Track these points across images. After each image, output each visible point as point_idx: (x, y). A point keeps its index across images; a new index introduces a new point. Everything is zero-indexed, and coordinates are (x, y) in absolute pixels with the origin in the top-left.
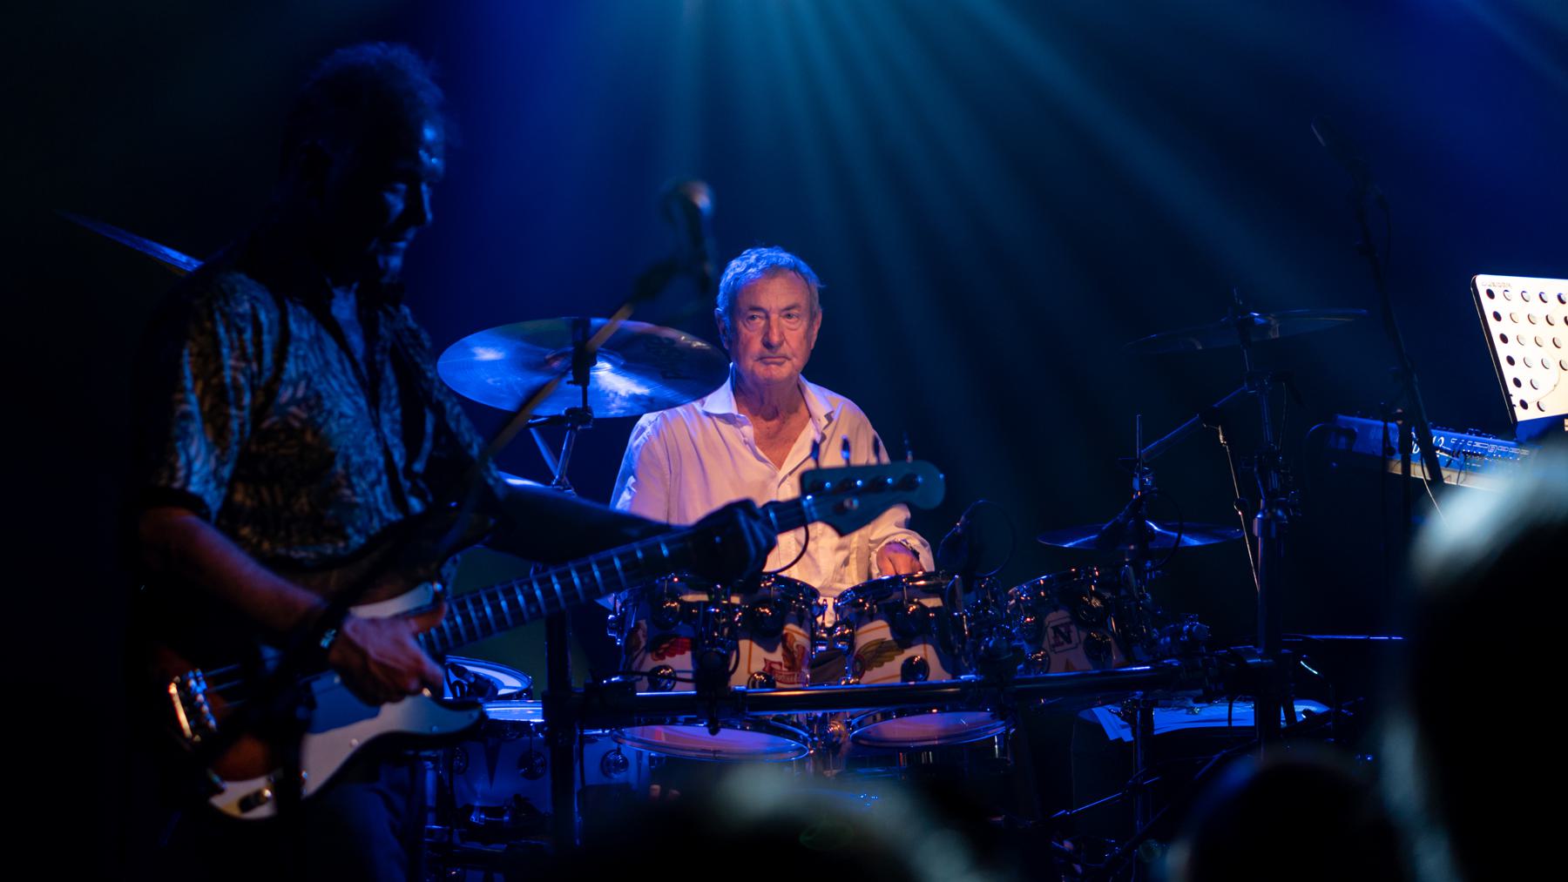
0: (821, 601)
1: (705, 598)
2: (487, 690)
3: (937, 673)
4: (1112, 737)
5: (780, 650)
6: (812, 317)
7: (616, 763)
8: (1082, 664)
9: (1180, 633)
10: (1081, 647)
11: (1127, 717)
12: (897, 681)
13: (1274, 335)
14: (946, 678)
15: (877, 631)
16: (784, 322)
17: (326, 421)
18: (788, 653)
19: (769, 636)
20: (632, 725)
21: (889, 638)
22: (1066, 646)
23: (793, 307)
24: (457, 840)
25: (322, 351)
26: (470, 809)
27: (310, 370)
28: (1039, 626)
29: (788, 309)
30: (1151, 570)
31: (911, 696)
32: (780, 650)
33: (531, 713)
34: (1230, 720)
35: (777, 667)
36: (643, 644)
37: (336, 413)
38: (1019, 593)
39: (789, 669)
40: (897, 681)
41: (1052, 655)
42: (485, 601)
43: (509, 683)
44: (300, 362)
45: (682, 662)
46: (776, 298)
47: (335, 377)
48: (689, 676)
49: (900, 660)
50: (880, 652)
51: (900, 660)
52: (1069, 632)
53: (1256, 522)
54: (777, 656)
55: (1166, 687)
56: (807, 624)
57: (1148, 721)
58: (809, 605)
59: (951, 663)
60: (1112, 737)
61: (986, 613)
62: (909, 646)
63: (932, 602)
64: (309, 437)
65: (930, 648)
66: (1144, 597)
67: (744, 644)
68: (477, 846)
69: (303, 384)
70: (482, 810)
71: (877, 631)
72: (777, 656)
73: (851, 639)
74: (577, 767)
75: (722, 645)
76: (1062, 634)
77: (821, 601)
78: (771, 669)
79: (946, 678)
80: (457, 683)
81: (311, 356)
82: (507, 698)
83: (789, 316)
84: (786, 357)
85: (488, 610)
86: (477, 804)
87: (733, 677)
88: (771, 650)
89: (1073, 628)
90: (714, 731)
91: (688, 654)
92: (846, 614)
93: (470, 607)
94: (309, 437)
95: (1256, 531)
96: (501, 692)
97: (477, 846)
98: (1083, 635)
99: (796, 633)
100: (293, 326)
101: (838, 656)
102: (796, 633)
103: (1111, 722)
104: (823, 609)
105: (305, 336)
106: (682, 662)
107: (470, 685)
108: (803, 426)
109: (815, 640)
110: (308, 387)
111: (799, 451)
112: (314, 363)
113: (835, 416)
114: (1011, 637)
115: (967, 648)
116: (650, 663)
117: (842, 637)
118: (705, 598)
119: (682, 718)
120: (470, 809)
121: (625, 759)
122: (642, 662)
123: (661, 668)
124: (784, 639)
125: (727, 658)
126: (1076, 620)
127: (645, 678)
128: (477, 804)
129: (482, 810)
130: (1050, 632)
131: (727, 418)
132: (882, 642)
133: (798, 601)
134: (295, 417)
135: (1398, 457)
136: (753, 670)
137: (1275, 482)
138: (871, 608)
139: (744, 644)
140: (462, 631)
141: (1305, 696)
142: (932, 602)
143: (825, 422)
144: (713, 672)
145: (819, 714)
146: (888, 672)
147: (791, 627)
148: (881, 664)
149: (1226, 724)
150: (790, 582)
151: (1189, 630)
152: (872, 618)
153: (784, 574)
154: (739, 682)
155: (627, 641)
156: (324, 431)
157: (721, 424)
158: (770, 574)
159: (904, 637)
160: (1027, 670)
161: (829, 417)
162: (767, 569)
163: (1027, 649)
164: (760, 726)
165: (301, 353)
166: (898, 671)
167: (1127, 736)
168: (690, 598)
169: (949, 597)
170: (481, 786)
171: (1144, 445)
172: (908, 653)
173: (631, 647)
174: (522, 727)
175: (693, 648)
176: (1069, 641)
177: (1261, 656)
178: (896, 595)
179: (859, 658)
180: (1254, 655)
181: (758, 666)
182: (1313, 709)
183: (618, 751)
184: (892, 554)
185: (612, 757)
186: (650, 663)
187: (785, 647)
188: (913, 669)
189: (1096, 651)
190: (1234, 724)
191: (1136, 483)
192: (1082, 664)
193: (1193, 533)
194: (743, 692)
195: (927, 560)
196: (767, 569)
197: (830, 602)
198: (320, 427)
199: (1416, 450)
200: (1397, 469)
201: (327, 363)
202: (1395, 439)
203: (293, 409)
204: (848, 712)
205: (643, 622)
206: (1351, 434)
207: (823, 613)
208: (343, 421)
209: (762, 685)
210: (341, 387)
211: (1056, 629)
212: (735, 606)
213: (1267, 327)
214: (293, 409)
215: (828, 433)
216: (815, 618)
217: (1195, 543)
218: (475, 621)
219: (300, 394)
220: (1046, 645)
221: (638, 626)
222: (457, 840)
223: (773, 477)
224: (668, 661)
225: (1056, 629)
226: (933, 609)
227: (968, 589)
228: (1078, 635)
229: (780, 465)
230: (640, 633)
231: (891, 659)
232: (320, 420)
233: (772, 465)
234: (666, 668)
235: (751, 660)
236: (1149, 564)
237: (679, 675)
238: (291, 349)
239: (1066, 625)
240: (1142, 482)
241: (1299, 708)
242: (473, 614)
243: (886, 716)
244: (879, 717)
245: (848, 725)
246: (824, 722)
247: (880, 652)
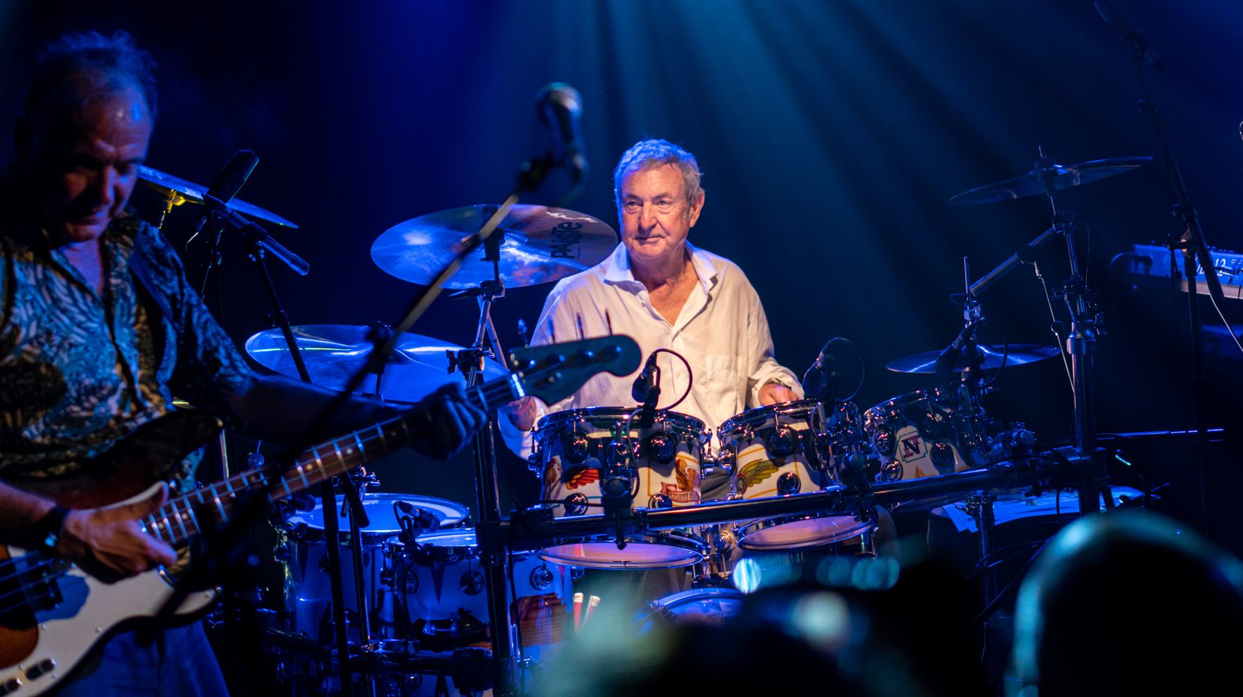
0: (706, 431)
1: (608, 434)
2: (428, 522)
3: (808, 486)
4: (960, 528)
5: (674, 473)
6: (690, 200)
7: (543, 578)
8: (929, 470)
9: (1010, 438)
10: (928, 456)
11: (974, 513)
12: (775, 494)
13: (1077, 183)
14: (815, 489)
15: (754, 454)
16: (655, 207)
17: (56, 354)
18: (681, 476)
19: (663, 461)
20: (552, 545)
21: (766, 458)
22: (916, 456)
23: (664, 195)
24: (412, 650)
25: (50, 291)
26: (422, 623)
27: (39, 311)
28: (892, 442)
29: (659, 197)
30: (983, 387)
31: (787, 507)
32: (674, 473)
33: (467, 538)
34: (1058, 508)
35: (672, 489)
36: (559, 476)
37: (66, 345)
38: (870, 415)
39: (683, 489)
40: (775, 494)
41: (903, 463)
42: (163, 514)
43: (451, 514)
44: (29, 306)
45: (592, 490)
46: (659, 187)
47: (64, 311)
48: (599, 501)
49: (776, 476)
50: (759, 471)
51: (776, 476)
52: (917, 444)
53: (1069, 341)
54: (672, 479)
55: (1002, 483)
56: (695, 450)
57: (988, 511)
58: (697, 435)
59: (819, 477)
60: (960, 528)
61: (845, 432)
62: (783, 464)
63: (801, 426)
64: (43, 370)
65: (800, 465)
66: (978, 411)
67: (643, 472)
68: (429, 653)
69: (34, 324)
70: (432, 623)
71: (754, 454)
72: (672, 479)
73: (733, 461)
74: (508, 583)
75: (625, 473)
76: (911, 446)
77: (706, 431)
78: (668, 491)
79: (815, 489)
80: (405, 518)
81: (39, 298)
82: (449, 527)
83: (663, 202)
84: (660, 236)
85: (166, 521)
86: (428, 618)
87: (635, 500)
88: (667, 474)
89: (920, 440)
90: (621, 547)
91: (597, 482)
92: (729, 440)
93: (175, 509)
94: (43, 370)
95: (1069, 350)
96: (442, 523)
97: (429, 653)
98: (929, 446)
99: (687, 460)
100: (19, 274)
101: (726, 474)
102: (687, 460)
103: (958, 514)
104: (709, 437)
105: (32, 281)
106: (592, 490)
107: (416, 519)
108: (692, 288)
109: (703, 464)
110: (38, 326)
111: (689, 309)
112: (44, 302)
113: (720, 279)
114: (869, 451)
115: (832, 463)
116: (565, 492)
117: (726, 460)
118: (608, 434)
119: (594, 537)
120: (422, 623)
121: (550, 573)
122: (558, 492)
123: (573, 496)
124: (677, 464)
125: (627, 485)
126: (922, 434)
127: (562, 506)
128: (428, 618)
129: (432, 623)
130: (901, 445)
131: (624, 286)
132: (760, 462)
133: (687, 432)
134: (29, 353)
135: (1185, 277)
136: (652, 493)
137: (1081, 308)
138: (749, 435)
139: (643, 472)
140: (171, 532)
141: (1121, 483)
142: (801, 426)
143: (710, 284)
144: (617, 498)
145: (711, 526)
146: (765, 488)
147: (682, 455)
148: (760, 481)
149: (1055, 512)
150: (679, 417)
151: (1018, 437)
152: (750, 442)
153: (674, 410)
154: (640, 502)
155: (545, 474)
156: (55, 363)
157: (621, 291)
158: (662, 411)
159: (779, 455)
160: (884, 477)
161: (714, 280)
162: (659, 407)
163: (883, 460)
164: (660, 540)
165: (29, 297)
166: (775, 487)
167: (973, 527)
168: (595, 435)
169: (814, 421)
170: (430, 602)
171: (971, 282)
172: (782, 470)
173: (548, 481)
174: (461, 551)
175: (601, 477)
176: (917, 451)
177: (1079, 454)
178: (769, 422)
179: (741, 477)
180: (1074, 454)
181: (657, 489)
182: (1129, 494)
183: (544, 567)
184: (771, 390)
185: (538, 572)
186: (565, 492)
187: (678, 471)
188: (787, 483)
189: (942, 459)
190: (1062, 511)
191: (967, 316)
192: (929, 470)
193: (1016, 352)
194: (644, 512)
195: (799, 392)
196: (659, 407)
197: (714, 433)
198: (52, 359)
199: (1201, 271)
200: (1186, 288)
201: (56, 301)
202: (1180, 261)
203: (27, 347)
204: (735, 523)
205: (558, 458)
206: (1147, 261)
207: (708, 440)
208: (73, 351)
209: (660, 505)
210: (72, 319)
211: (906, 442)
212: (634, 439)
213: (1068, 177)
214: (27, 347)
215: (713, 293)
216: (702, 445)
217: (1021, 361)
218: (180, 521)
219: (32, 333)
220: (898, 456)
221: (553, 461)
222: (412, 650)
223: (668, 333)
224: (580, 489)
225: (906, 442)
226: (801, 432)
227: (828, 413)
228: (925, 446)
229: (673, 322)
230: (556, 467)
231: (768, 476)
232: (51, 354)
233: (666, 323)
234: (579, 495)
235: (649, 486)
236: (981, 382)
237: (590, 501)
238: (19, 296)
239: (914, 438)
240: (971, 314)
241: (1116, 494)
242: (178, 516)
243: (767, 524)
244: (761, 525)
245: (736, 533)
246: (715, 530)
247: (759, 471)
